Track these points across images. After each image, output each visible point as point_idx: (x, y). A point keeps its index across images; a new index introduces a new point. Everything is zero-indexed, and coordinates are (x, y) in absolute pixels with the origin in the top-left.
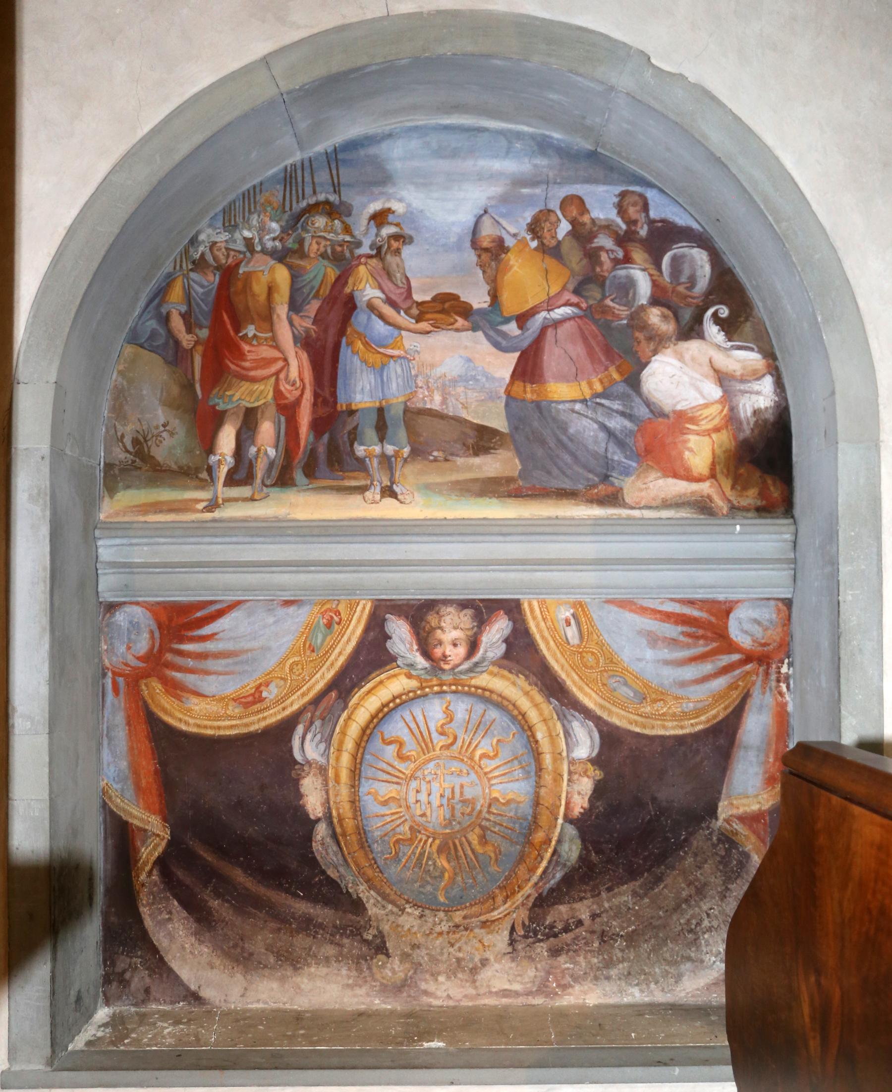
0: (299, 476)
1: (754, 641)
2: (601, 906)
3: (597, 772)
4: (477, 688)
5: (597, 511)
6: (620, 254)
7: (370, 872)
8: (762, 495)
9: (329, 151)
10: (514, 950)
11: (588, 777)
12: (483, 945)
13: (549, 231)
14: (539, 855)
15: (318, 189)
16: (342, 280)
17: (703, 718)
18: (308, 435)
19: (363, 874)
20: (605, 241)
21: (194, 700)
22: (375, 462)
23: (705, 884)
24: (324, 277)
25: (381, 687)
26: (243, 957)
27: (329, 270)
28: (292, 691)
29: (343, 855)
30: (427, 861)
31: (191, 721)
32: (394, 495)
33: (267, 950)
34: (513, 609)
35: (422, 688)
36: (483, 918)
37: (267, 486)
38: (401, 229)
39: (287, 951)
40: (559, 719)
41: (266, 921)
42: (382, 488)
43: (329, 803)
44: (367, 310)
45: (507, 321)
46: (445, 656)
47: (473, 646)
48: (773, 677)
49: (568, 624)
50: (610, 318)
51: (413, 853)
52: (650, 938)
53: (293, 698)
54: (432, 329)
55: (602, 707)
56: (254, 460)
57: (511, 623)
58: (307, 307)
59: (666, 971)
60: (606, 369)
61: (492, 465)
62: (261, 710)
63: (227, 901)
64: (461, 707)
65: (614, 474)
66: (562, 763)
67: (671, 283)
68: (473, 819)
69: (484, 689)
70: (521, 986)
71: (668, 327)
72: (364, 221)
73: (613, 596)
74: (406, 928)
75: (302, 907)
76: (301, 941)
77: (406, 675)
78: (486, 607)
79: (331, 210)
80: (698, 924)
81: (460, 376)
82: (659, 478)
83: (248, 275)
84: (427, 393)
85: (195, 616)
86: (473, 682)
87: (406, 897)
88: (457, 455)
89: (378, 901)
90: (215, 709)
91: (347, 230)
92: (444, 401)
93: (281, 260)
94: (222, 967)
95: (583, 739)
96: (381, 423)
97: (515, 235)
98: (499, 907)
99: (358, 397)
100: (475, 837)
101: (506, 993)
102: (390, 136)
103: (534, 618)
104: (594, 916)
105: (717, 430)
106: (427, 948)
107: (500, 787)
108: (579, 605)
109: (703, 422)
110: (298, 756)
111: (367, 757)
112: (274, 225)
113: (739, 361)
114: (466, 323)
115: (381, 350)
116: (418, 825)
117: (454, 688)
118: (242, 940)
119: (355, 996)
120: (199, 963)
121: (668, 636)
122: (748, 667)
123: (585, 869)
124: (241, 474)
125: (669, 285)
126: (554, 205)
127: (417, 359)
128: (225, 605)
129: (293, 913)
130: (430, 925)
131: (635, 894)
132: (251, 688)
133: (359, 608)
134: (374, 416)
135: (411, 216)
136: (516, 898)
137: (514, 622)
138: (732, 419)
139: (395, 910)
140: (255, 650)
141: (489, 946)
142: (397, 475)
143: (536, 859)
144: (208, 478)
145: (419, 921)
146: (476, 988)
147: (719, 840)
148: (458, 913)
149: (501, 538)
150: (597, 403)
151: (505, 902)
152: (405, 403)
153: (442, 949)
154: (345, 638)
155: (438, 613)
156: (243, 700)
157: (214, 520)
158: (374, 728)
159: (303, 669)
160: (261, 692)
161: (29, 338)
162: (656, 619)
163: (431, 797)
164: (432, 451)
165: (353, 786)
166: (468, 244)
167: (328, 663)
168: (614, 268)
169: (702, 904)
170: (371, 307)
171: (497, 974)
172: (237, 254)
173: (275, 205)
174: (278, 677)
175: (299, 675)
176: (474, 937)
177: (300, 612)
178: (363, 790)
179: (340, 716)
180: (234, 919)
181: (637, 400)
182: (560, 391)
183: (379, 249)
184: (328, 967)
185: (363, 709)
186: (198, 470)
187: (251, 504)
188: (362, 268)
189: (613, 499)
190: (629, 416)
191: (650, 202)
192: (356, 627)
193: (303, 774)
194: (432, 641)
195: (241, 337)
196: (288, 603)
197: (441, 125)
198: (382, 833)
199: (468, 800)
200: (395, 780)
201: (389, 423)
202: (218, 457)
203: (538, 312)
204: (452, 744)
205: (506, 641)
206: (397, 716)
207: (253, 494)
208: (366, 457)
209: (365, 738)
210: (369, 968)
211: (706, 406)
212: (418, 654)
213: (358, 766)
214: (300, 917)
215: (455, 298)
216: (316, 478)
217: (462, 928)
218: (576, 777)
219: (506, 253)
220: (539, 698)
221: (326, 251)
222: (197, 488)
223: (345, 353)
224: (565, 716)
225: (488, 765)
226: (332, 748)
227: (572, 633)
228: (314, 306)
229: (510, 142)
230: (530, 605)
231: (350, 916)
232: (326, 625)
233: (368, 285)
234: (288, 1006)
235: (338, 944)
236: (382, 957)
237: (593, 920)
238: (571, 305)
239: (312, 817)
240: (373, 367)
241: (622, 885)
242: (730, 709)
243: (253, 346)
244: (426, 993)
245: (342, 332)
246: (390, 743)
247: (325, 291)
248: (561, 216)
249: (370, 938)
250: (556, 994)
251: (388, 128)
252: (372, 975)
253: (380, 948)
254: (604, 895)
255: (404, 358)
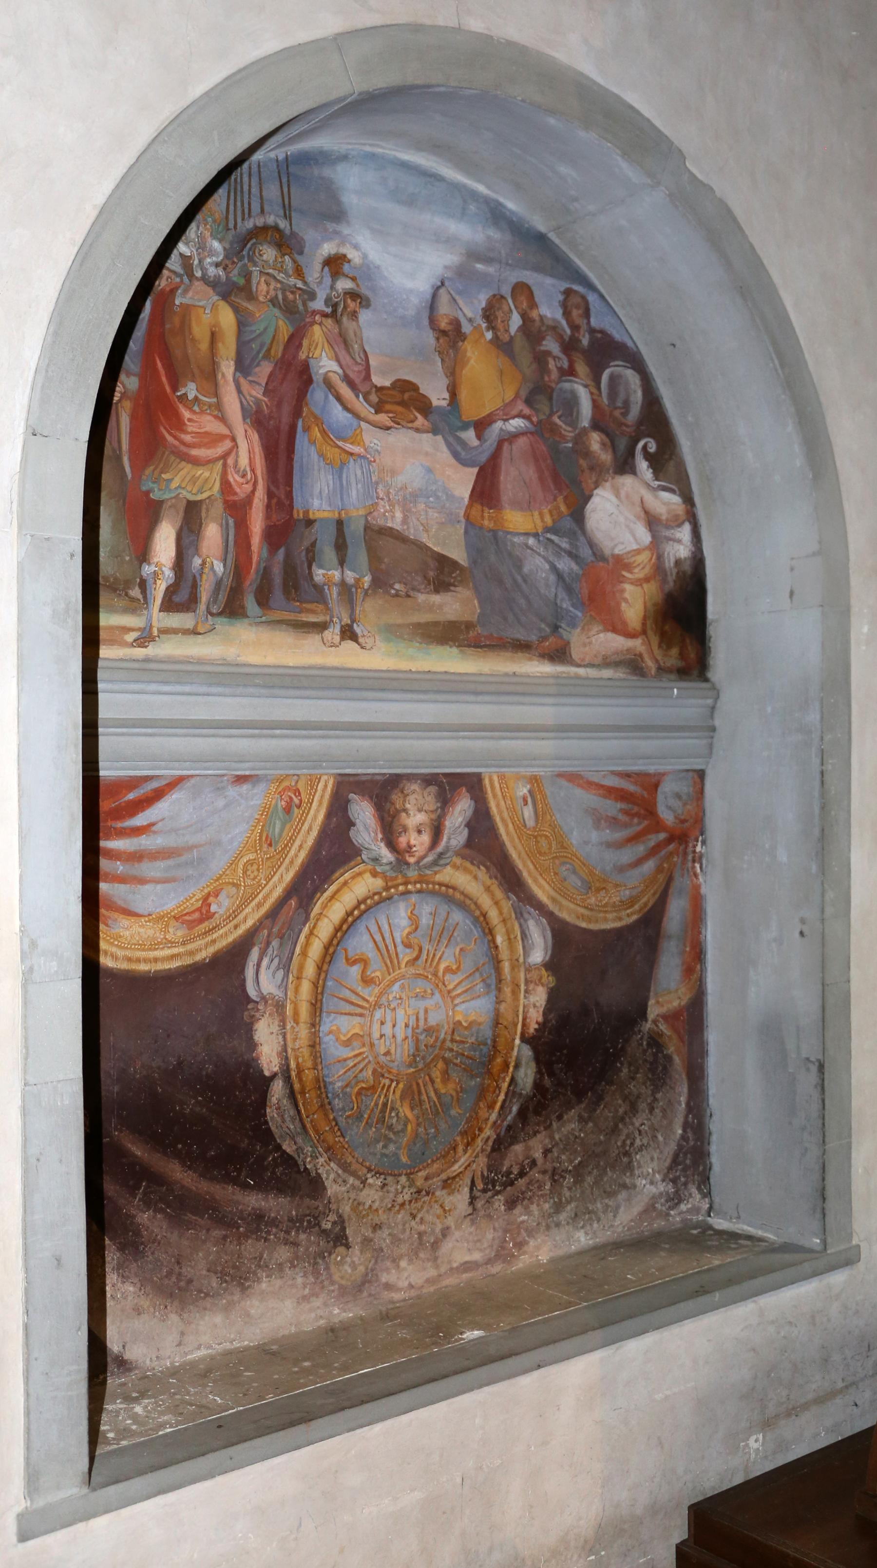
0: (250, 603)
1: (676, 818)
2: (552, 1138)
3: (550, 978)
4: (441, 884)
5: (547, 668)
6: (566, 365)
7: (330, 1139)
8: (682, 656)
9: (280, 158)
10: (474, 1209)
11: (543, 985)
12: (445, 1210)
13: (503, 322)
14: (497, 1085)
15: (267, 208)
16: (295, 339)
17: (637, 907)
18: (260, 548)
19: (323, 1141)
20: (551, 345)
21: (124, 921)
22: (335, 590)
23: (638, 1097)
24: (276, 331)
25: (345, 889)
26: (180, 1289)
27: (281, 323)
28: (245, 902)
29: (301, 1120)
30: (390, 1113)
31: (120, 953)
32: (354, 637)
33: (208, 1271)
34: (473, 784)
35: (387, 888)
36: (444, 1176)
37: (212, 614)
38: (358, 285)
39: (234, 1267)
40: (516, 918)
41: (208, 1230)
42: (342, 627)
43: (286, 1051)
44: (323, 386)
45: (465, 427)
46: (410, 847)
47: (437, 832)
48: (690, 857)
49: (526, 803)
50: (558, 439)
51: (376, 1105)
52: (593, 1169)
53: (247, 910)
54: (392, 424)
55: (554, 900)
56: (198, 576)
57: (473, 803)
58: (257, 369)
59: (606, 1204)
60: (555, 499)
61: (453, 605)
62: (210, 930)
63: (161, 1211)
64: (426, 909)
65: (563, 625)
66: (519, 971)
67: (608, 406)
68: (436, 1052)
69: (447, 886)
70: (481, 1254)
71: (606, 457)
72: (318, 267)
73: (565, 769)
74: (367, 1207)
75: (254, 1201)
76: (250, 1247)
77: (371, 873)
78: (449, 783)
79: (286, 243)
80: (632, 1144)
81: (420, 490)
82: (601, 631)
83: (187, 309)
84: (388, 508)
85: (126, 799)
86: (438, 878)
87: (368, 1164)
88: (419, 591)
89: (339, 1175)
90: (151, 932)
91: (299, 272)
92: (405, 521)
93: (225, 296)
94: (152, 1310)
95: (538, 940)
96: (341, 541)
97: (470, 320)
98: (460, 1158)
99: (316, 503)
100: (438, 1073)
101: (467, 1267)
102: (344, 158)
103: (495, 796)
104: (546, 1152)
105: (647, 580)
106: (389, 1227)
107: (463, 1006)
108: (534, 780)
109: (636, 570)
110: (252, 992)
111: (330, 983)
112: (216, 245)
113: (664, 504)
114: (426, 423)
115: (340, 443)
116: (382, 1067)
117: (418, 886)
118: (178, 1263)
119: (311, 1310)
120: (123, 1311)
121: (609, 815)
122: (672, 847)
123: (539, 1097)
124: (182, 596)
125: (606, 408)
126: (506, 291)
127: (377, 461)
128: (164, 783)
129: (242, 1211)
130: (391, 1195)
131: (581, 1119)
132: (197, 901)
133: (321, 786)
134: (333, 530)
135: (368, 271)
136: (476, 1145)
137: (476, 802)
138: (659, 569)
139: (357, 1183)
140: (201, 846)
141: (450, 1211)
142: (357, 612)
143: (494, 1092)
144: (140, 597)
145: (381, 1193)
146: (437, 1267)
147: (649, 1044)
148: (420, 1174)
149: (472, 698)
150: (548, 539)
151: (465, 1151)
152: (366, 516)
153: (404, 1225)
154: (306, 826)
155: (402, 792)
156: (187, 918)
157: (147, 660)
158: (338, 944)
159: (258, 870)
160: (209, 905)
161: (48, 365)
162: (600, 795)
163: (396, 1028)
164: (394, 583)
165: (313, 1025)
166: (426, 322)
167: (287, 861)
168: (560, 381)
169: (634, 1120)
170: (328, 383)
171: (458, 1244)
172: (173, 276)
173: (217, 216)
174: (229, 883)
175: (254, 879)
176: (436, 1201)
177: (255, 791)
178: (324, 1028)
179: (300, 931)
180: (169, 1235)
181: (582, 538)
182: (517, 520)
183: (335, 306)
184: (282, 1277)
185: (326, 920)
186: (128, 584)
187: (191, 639)
188: (316, 329)
189: (559, 654)
190: (573, 555)
191: (591, 307)
192: (318, 811)
193: (258, 1015)
194: (397, 828)
195: (178, 397)
196: (240, 779)
197: (398, 159)
198: (344, 1083)
199: (432, 1027)
200: (359, 1010)
201: (348, 541)
202: (153, 568)
203: (495, 421)
204: (417, 958)
205: (468, 825)
206: (361, 926)
207: (196, 626)
208: (325, 584)
209: (328, 958)
210: (327, 1268)
211: (638, 552)
212: (382, 845)
213: (319, 997)
214: (249, 1215)
215: (414, 388)
216: (270, 608)
217: (424, 1192)
218: (531, 987)
219: (463, 341)
220: (499, 894)
221: (276, 296)
222: (126, 611)
223: (301, 440)
224: (522, 914)
225: (452, 981)
226: (291, 976)
227: (528, 812)
228: (265, 369)
229: (465, 201)
230: (491, 780)
231: (307, 1201)
232: (284, 809)
233: (324, 353)
234: (236, 1344)
235: (295, 1244)
236: (341, 1249)
237: (545, 1157)
238: (524, 417)
239: (267, 1073)
240: (331, 464)
241: (570, 1110)
242: (657, 896)
243: (194, 412)
244: (388, 1287)
245: (297, 413)
246: (354, 963)
247: (278, 351)
248: (513, 307)
249: (328, 1226)
250: (513, 1256)
251: (345, 147)
252: (330, 1276)
253: (340, 1239)
254: (555, 1125)
255: (364, 457)
